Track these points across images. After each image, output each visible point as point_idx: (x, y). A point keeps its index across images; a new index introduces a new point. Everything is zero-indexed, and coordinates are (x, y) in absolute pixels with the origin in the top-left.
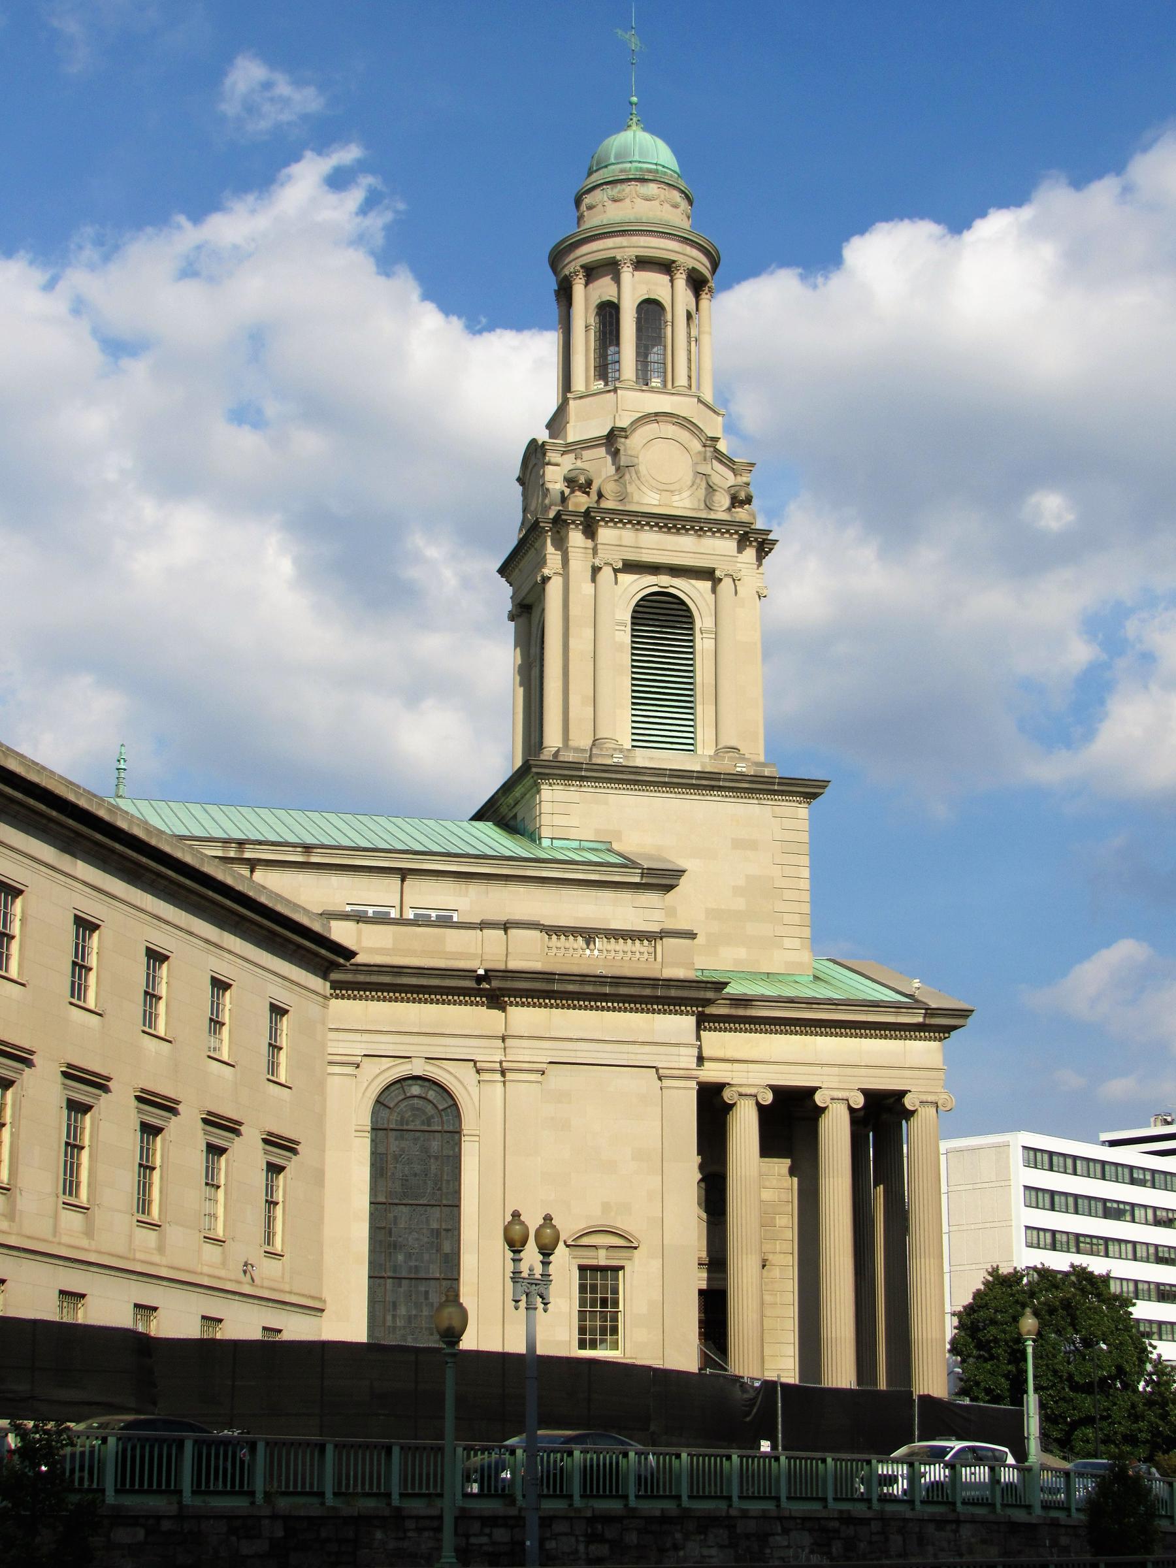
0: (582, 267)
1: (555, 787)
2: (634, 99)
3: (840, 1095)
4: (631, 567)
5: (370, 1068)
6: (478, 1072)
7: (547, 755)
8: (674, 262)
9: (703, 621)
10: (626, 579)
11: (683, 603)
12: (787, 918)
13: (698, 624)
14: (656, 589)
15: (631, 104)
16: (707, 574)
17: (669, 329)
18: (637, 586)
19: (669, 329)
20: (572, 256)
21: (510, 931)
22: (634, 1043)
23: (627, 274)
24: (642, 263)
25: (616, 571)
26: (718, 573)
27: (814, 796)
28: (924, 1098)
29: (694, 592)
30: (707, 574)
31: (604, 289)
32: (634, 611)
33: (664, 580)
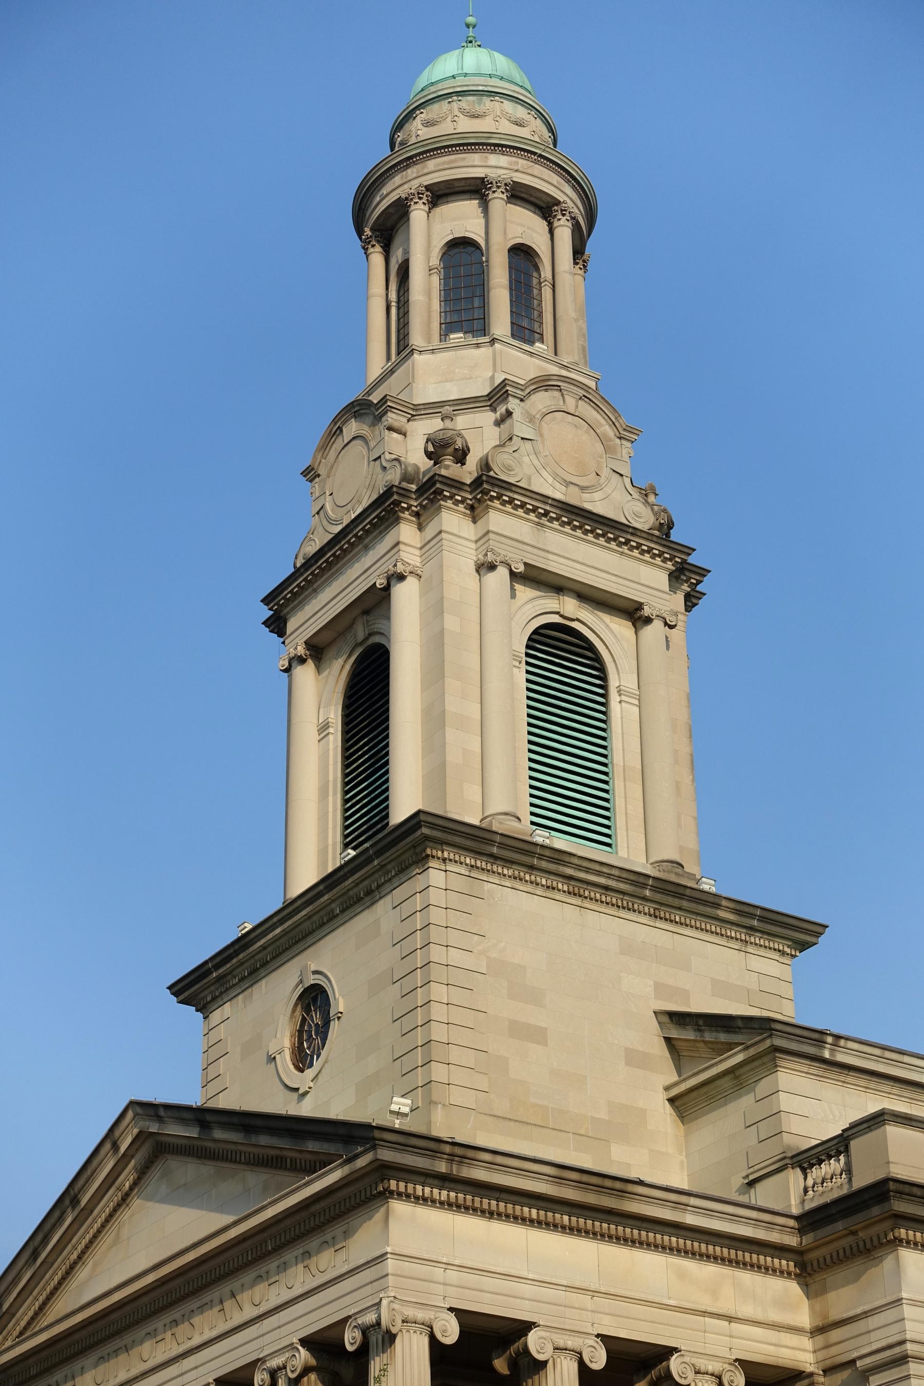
0: (428, 188)
1: (451, 867)
2: (471, 20)
8: (558, 203)
9: (621, 677)
10: (525, 592)
11: (591, 647)
12: (467, 1058)
13: (613, 682)
14: (556, 619)
15: (468, 26)
16: (634, 614)
18: (536, 608)
20: (384, 191)
21: (434, 1098)
23: (498, 200)
24: (519, 194)
25: (513, 574)
29: (608, 633)
31: (462, 217)
32: (530, 639)
33: (570, 606)
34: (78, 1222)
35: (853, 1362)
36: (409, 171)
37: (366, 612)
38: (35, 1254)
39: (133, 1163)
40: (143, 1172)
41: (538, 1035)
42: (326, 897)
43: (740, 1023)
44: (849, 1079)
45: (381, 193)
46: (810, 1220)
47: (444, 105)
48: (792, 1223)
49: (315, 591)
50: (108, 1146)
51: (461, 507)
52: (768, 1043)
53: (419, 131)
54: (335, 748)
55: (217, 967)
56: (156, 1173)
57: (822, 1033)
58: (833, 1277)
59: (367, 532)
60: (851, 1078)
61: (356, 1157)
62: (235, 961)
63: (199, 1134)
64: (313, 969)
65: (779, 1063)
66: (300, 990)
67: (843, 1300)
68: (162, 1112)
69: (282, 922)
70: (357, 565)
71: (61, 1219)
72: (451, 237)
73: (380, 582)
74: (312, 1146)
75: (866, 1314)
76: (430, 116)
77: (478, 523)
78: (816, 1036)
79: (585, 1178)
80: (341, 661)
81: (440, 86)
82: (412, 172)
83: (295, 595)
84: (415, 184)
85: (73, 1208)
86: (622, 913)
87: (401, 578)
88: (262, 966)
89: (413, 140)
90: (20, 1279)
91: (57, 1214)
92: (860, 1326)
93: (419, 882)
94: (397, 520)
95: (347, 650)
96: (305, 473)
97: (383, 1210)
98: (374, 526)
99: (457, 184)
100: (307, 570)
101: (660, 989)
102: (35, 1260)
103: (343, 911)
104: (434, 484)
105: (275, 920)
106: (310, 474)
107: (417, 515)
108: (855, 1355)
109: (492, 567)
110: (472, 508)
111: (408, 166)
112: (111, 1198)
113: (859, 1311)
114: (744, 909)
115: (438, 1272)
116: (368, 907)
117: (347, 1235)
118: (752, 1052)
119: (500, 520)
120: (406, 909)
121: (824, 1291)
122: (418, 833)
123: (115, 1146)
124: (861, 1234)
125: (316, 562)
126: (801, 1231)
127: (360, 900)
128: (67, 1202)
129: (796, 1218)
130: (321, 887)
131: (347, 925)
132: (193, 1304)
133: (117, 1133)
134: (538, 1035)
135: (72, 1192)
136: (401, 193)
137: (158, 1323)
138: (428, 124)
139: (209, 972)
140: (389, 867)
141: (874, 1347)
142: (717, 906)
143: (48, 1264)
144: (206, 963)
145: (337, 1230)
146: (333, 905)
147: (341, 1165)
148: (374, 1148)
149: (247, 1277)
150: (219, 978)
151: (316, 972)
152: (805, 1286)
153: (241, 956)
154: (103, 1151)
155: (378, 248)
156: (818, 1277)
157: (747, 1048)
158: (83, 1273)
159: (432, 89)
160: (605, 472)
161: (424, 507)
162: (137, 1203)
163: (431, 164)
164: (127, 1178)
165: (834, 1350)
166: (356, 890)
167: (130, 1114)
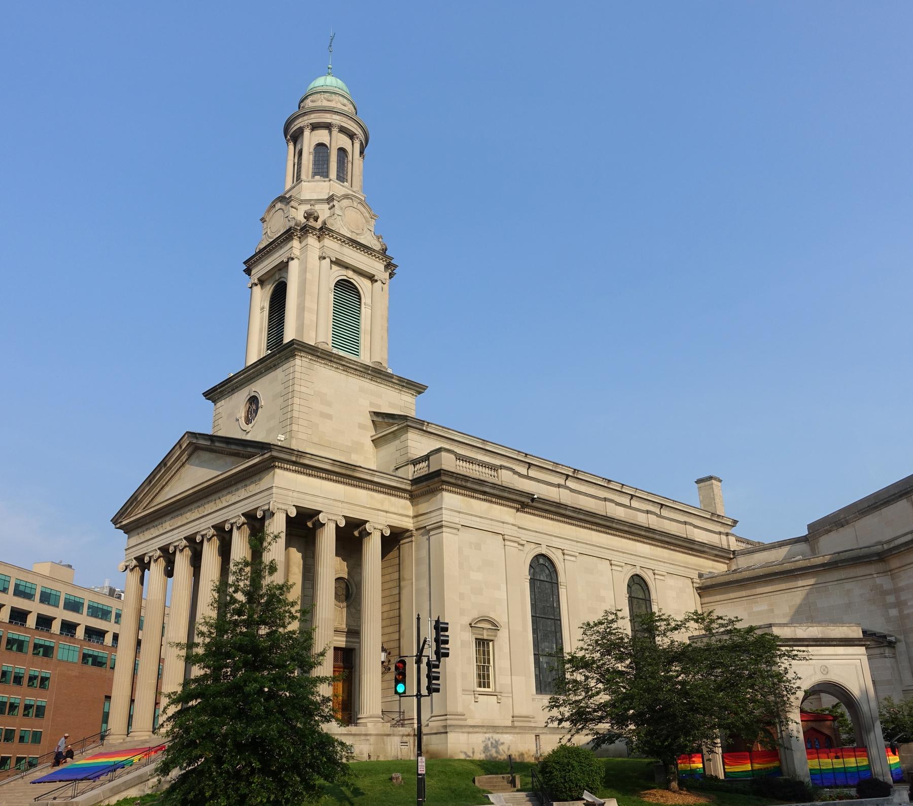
3: (283, 507)
4: (338, 263)
5: (528, 547)
6: (564, 554)
7: (287, 340)
10: (335, 268)
11: (356, 288)
14: (345, 278)
16: (372, 278)
17: (350, 165)
18: (339, 273)
19: (350, 165)
22: (472, 515)
23: (335, 131)
24: (343, 130)
26: (376, 278)
27: (420, 393)
28: (280, 506)
29: (363, 284)
30: (372, 278)
33: (350, 274)
37: (280, 270)
38: (150, 482)
40: (190, 456)
41: (329, 417)
46: (415, 482)
56: (195, 455)
58: (421, 500)
67: (423, 507)
71: (160, 470)
74: (249, 450)
82: (306, 118)
87: (293, 259)
93: (292, 363)
94: (293, 239)
101: (371, 404)
109: (324, 258)
112: (178, 464)
115: (290, 493)
119: (328, 242)
120: (287, 372)
121: (417, 504)
123: (181, 447)
126: (412, 485)
134: (329, 417)
138: (313, 101)
143: (154, 485)
145: (257, 478)
158: (167, 489)
160: (365, 229)
162: (187, 466)
163: (313, 116)
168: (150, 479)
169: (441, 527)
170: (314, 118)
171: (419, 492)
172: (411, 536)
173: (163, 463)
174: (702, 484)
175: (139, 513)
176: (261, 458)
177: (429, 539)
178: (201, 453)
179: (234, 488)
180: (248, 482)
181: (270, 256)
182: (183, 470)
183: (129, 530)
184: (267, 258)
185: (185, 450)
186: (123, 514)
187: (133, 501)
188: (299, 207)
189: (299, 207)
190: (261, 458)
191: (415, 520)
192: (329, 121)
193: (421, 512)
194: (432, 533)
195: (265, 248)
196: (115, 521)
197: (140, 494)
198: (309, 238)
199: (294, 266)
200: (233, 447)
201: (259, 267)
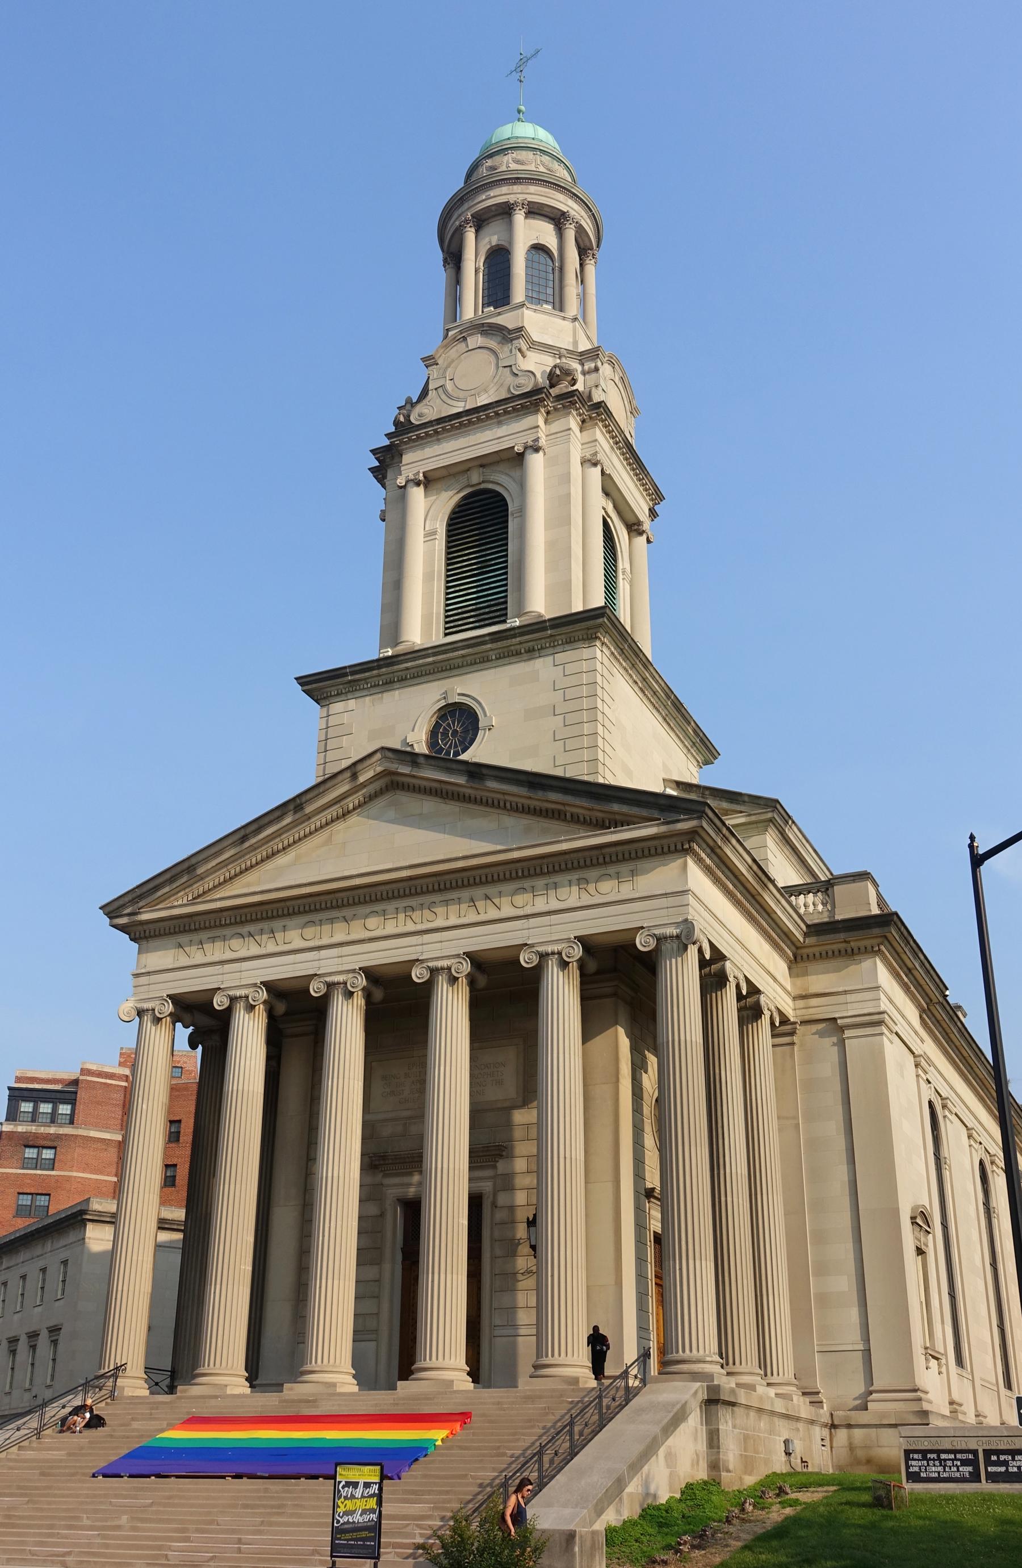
2: (522, 108)
20: (492, 193)
34: (294, 824)
35: (835, 1019)
36: (515, 187)
37: (482, 466)
38: (244, 839)
39: (365, 790)
40: (371, 798)
42: (489, 646)
43: (746, 799)
44: (785, 850)
45: (488, 193)
46: (815, 930)
47: (530, 154)
48: (804, 928)
49: (438, 440)
50: (348, 774)
51: (578, 419)
52: (770, 815)
53: (507, 163)
54: (440, 550)
55: (353, 673)
56: (381, 802)
57: (790, 817)
58: (812, 966)
59: (506, 412)
60: (787, 850)
61: (678, 821)
62: (375, 672)
63: (467, 781)
64: (458, 691)
65: (769, 830)
66: (443, 703)
67: (820, 981)
68: (421, 760)
69: (435, 654)
70: (488, 432)
71: (280, 818)
72: (536, 242)
73: (519, 449)
74: (616, 807)
75: (845, 992)
76: (519, 157)
77: (584, 433)
78: (787, 818)
79: (760, 874)
80: (451, 493)
81: (520, 140)
82: (517, 188)
83: (419, 437)
84: (521, 197)
85: (295, 812)
86: (654, 712)
87: (537, 450)
88: (398, 681)
89: (504, 168)
90: (221, 854)
91: (278, 813)
92: (841, 999)
93: (586, 653)
94: (537, 411)
95: (459, 487)
96: (424, 360)
97: (680, 861)
98: (515, 409)
99: (546, 209)
100: (438, 424)
102: (243, 842)
103: (497, 659)
104: (573, 396)
105: (430, 651)
106: (429, 361)
107: (548, 413)
108: (836, 1016)
109: (595, 465)
110: (583, 421)
111: (515, 184)
112: (328, 815)
113: (841, 989)
114: (698, 731)
116: (525, 661)
117: (633, 873)
118: (753, 818)
120: (570, 669)
121: (805, 974)
122: (601, 620)
124: (852, 944)
125: (450, 421)
126: (806, 935)
127: (518, 653)
128: (291, 807)
129: (808, 926)
130: (487, 638)
131: (498, 669)
132: (437, 898)
133: (359, 767)
135: (298, 801)
136: (512, 199)
137: (390, 906)
138: (517, 162)
139: (345, 675)
140: (558, 637)
141: (850, 1014)
142: (689, 723)
143: (253, 848)
144: (345, 668)
145: (624, 868)
146: (491, 653)
147: (658, 825)
148: (700, 818)
149: (509, 887)
150: (350, 682)
151: (459, 694)
152: (789, 968)
153: (384, 670)
154: (340, 778)
155: (473, 229)
156: (802, 965)
157: (750, 815)
158: (281, 860)
159: (508, 142)
161: (556, 409)
162: (354, 819)
163: (532, 189)
164: (351, 802)
165: (811, 1011)
166: (518, 647)
167: (378, 756)
168: (243, 835)
169: (880, 1023)
170: (537, 194)
171: (817, 950)
172: (792, 1034)
173: (296, 804)
174: (143, 980)
175: (179, 904)
176: (663, 829)
177: (842, 1044)
178: (404, 798)
179: (540, 882)
180: (592, 873)
181: (422, 447)
182: (340, 826)
183: (141, 934)
184: (456, 437)
185: (363, 785)
186: (141, 897)
187: (185, 870)
188: (529, 354)
189: (529, 354)
190: (663, 829)
191: (801, 1003)
192: (564, 209)
193: (813, 990)
194: (848, 1033)
195: (458, 415)
196: (112, 910)
197: (206, 860)
198: (571, 418)
199: (536, 462)
200: (553, 796)
201: (429, 451)
